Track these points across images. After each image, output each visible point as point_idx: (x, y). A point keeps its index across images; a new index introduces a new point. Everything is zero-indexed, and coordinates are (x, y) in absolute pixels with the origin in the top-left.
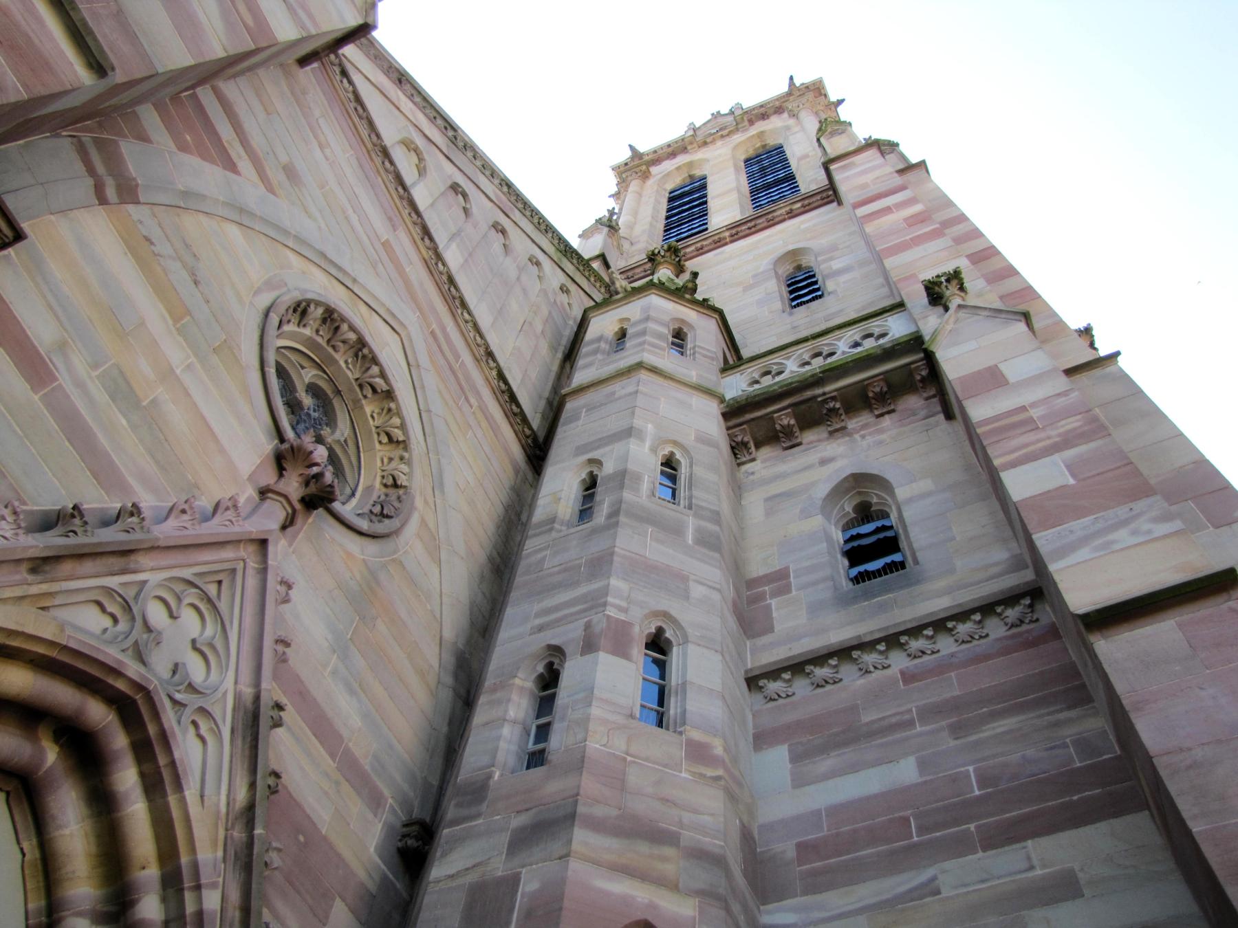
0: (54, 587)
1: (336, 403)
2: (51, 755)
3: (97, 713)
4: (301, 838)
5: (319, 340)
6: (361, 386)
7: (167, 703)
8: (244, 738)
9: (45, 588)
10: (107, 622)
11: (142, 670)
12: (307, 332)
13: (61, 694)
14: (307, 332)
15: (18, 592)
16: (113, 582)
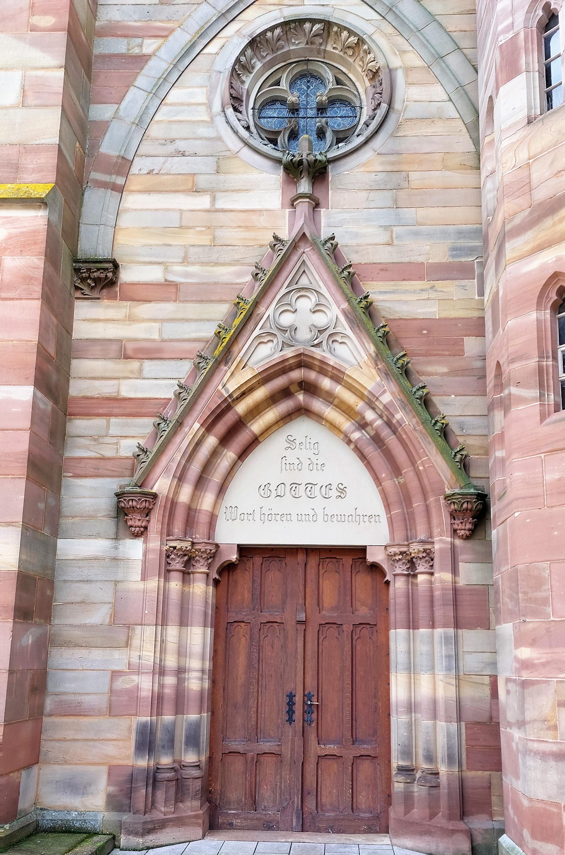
0: (238, 359)
1: (311, 67)
2: (301, 397)
3: (296, 375)
4: (425, 332)
5: (268, 58)
6: (312, 43)
7: (313, 349)
8: (152, 479)
9: (235, 364)
10: (270, 345)
11: (293, 348)
12: (259, 65)
13: (279, 382)
14: (259, 65)
15: (229, 374)
16: (257, 332)
